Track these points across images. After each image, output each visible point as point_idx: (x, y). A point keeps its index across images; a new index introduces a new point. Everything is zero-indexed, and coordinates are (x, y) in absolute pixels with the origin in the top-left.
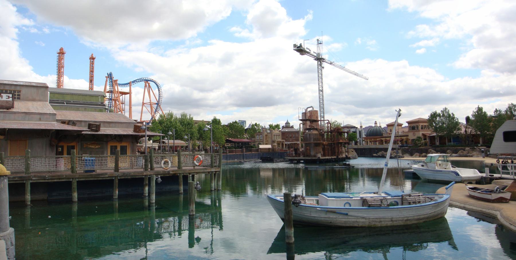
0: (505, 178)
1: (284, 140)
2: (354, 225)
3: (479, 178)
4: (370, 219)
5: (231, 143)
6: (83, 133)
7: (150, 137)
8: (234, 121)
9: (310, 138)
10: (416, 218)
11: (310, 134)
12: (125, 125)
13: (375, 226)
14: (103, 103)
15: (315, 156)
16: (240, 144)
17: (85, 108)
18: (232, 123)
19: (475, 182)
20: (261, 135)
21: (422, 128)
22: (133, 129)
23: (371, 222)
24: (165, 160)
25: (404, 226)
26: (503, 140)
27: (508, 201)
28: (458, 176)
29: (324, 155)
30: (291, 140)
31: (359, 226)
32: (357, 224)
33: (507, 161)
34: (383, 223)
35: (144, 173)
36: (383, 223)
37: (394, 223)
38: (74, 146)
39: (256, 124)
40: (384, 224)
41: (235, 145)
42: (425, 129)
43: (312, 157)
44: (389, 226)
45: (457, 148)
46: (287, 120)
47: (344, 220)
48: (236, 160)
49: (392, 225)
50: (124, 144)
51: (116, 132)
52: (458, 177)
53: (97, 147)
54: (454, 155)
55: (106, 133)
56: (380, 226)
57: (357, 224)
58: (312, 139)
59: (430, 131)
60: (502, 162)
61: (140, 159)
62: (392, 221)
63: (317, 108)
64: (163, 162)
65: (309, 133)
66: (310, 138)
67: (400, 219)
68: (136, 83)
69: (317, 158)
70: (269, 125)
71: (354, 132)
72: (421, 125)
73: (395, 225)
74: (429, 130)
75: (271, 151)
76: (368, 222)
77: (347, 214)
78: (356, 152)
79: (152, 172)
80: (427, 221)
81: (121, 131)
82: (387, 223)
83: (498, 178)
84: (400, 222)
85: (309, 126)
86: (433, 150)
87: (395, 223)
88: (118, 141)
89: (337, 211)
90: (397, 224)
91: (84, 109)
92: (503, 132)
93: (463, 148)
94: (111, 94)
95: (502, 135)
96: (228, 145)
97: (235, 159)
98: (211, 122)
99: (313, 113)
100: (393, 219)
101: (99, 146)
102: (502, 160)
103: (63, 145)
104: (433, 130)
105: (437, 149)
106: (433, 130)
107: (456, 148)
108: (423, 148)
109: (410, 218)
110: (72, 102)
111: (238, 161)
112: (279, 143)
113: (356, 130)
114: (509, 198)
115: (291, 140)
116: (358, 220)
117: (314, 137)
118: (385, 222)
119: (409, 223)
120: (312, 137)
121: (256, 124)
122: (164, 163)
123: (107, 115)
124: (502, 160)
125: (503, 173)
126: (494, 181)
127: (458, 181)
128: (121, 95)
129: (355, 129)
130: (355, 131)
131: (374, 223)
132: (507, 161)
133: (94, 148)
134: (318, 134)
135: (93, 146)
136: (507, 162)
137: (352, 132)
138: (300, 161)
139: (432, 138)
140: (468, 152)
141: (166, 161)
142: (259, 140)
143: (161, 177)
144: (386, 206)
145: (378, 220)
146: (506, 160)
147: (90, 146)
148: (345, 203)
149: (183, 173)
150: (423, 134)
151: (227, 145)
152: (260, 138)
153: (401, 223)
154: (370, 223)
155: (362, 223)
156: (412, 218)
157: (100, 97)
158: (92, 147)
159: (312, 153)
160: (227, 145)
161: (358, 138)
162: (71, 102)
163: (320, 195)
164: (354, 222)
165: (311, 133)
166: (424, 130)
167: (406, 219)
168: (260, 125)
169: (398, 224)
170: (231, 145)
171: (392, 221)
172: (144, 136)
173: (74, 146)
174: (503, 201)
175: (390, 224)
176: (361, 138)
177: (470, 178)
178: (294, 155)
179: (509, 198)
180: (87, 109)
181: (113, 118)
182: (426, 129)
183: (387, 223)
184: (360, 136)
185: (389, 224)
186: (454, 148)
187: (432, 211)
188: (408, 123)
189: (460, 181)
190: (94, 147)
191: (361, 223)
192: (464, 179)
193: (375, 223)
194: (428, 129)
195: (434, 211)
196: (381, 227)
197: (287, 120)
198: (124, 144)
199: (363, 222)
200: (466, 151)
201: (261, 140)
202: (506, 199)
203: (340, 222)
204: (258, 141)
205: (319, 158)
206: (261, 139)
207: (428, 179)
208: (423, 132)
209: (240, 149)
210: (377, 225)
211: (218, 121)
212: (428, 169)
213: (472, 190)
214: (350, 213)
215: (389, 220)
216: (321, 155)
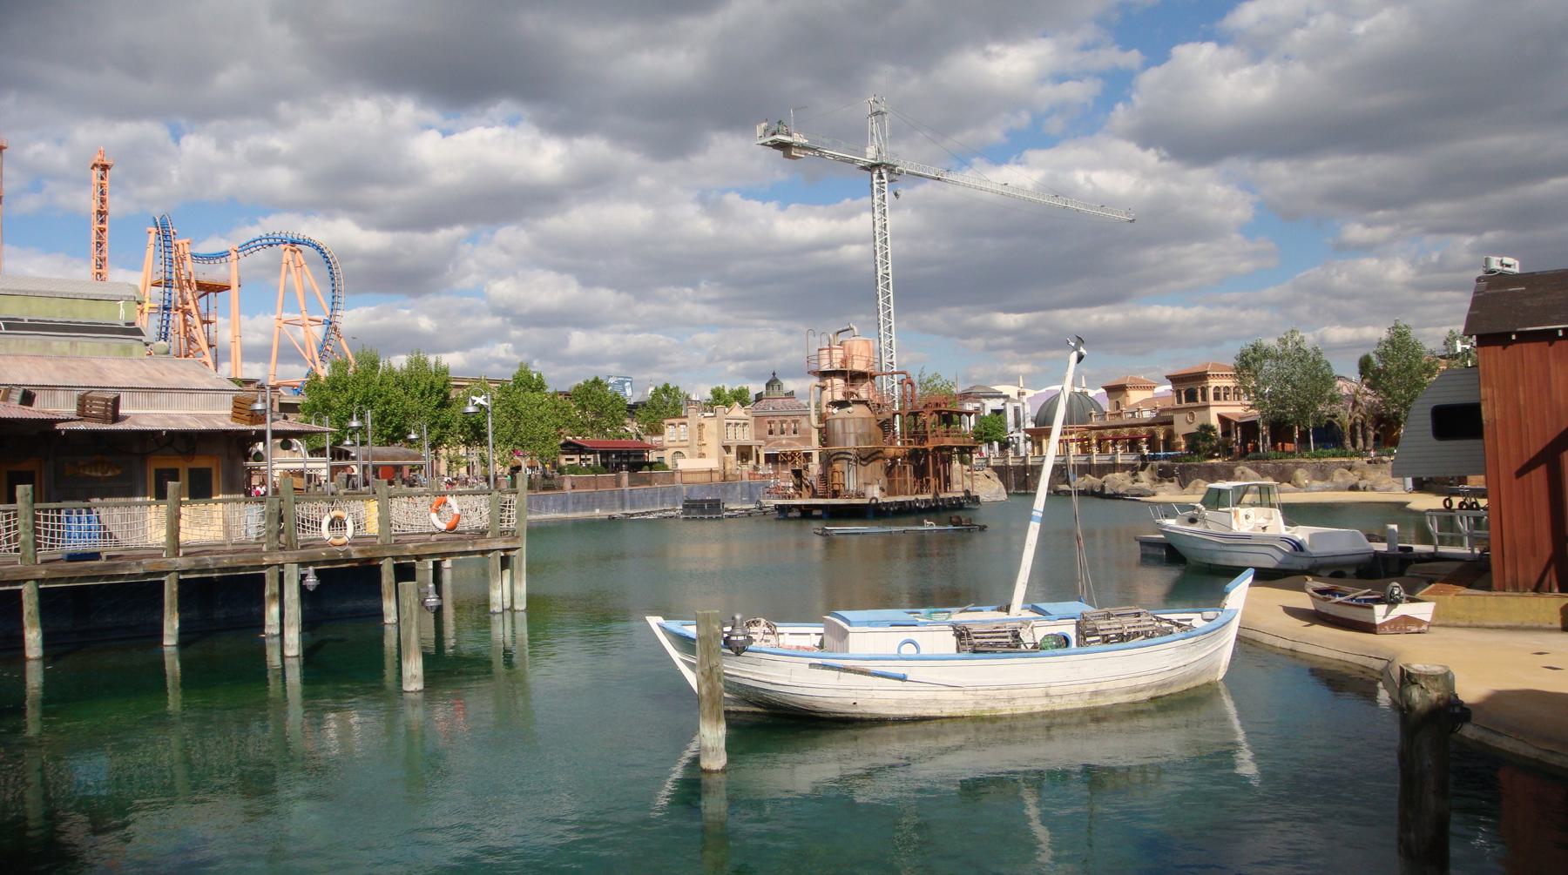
0: (1451, 557)
1: (763, 441)
2: (928, 711)
3: (1367, 556)
4: (978, 693)
5: (580, 454)
6: (59, 426)
7: (285, 439)
8: (591, 379)
9: (844, 432)
10: (1124, 684)
11: (843, 420)
12: (202, 396)
13: (993, 714)
14: (133, 324)
15: (860, 495)
16: (614, 456)
17: (72, 343)
18: (583, 384)
19: (1353, 571)
20: (682, 426)
21: (1217, 397)
22: (230, 412)
23: (981, 702)
24: (333, 514)
25: (1087, 711)
26: (1431, 433)
27: (1424, 627)
28: (1298, 553)
29: (891, 491)
30: (784, 442)
31: (944, 715)
32: (938, 709)
33: (1473, 503)
34: (1019, 702)
35: (265, 559)
36: (1019, 702)
37: (1054, 703)
38: (210, 469)
39: (667, 386)
40: (1022, 707)
41: (595, 459)
42: (1225, 399)
43: (850, 497)
44: (1038, 713)
45: (1325, 460)
46: (774, 374)
47: (896, 695)
48: (597, 511)
49: (1049, 709)
50: (201, 463)
51: (171, 422)
52: (1302, 554)
53: (110, 474)
54: (1317, 484)
55: (138, 428)
56: (1008, 712)
57: (938, 709)
58: (852, 437)
59: (1242, 405)
60: (1461, 505)
61: (252, 510)
62: (1047, 695)
63: (76, 394)
64: (326, 521)
65: (841, 415)
66: (844, 432)
67: (1074, 689)
68: (252, 250)
69: (866, 501)
70: (713, 392)
71: (997, 412)
72: (1214, 385)
73: (1057, 708)
74: (1238, 403)
75: (716, 477)
76: (971, 702)
77: (903, 679)
78: (1001, 478)
79: (291, 555)
80: (1160, 697)
81: (189, 418)
82: (1032, 702)
83: (1425, 556)
84: (1074, 698)
85: (844, 394)
86: (1251, 468)
87: (1059, 705)
88: (181, 453)
89: (873, 669)
90: (1063, 708)
91: (68, 343)
92: (1432, 406)
93: (1346, 460)
94: (167, 290)
95: (1429, 417)
96: (572, 460)
97: (593, 509)
98: (511, 383)
99: (858, 350)
100: (1052, 691)
101: (118, 472)
102: (1461, 499)
103: (176, 466)
104: (1250, 403)
105: (1263, 465)
106: (1250, 403)
107: (1323, 460)
108: (1217, 464)
109: (1103, 687)
110: (26, 322)
111: (605, 514)
112: (745, 450)
113: (1003, 404)
114: (1427, 618)
115: (784, 442)
116: (940, 696)
117: (860, 431)
118: (1026, 700)
119: (1101, 702)
120: (852, 430)
121: (667, 386)
122: (332, 523)
123: (143, 364)
124: (1461, 499)
125: (1442, 542)
126: (1412, 566)
127: (1300, 568)
128: (202, 292)
129: (1002, 401)
130: (1002, 408)
131: (989, 704)
132: (1476, 503)
133: (99, 478)
134: (870, 418)
135: (96, 471)
136: (1475, 506)
137: (992, 410)
138: (811, 511)
139: (1250, 429)
140: (1360, 473)
141: (339, 518)
142: (677, 444)
143: (317, 572)
144: (1030, 646)
145: (1005, 694)
146: (1473, 500)
147: (87, 473)
148: (903, 639)
149: (396, 558)
150: (1222, 418)
151: (567, 460)
152: (679, 437)
153: (1079, 704)
154: (977, 703)
155: (953, 706)
156: (1111, 685)
157: (121, 302)
158: (94, 474)
159: (852, 484)
160: (567, 460)
161: (1012, 433)
162: (22, 320)
163: (828, 617)
164: (927, 701)
165: (850, 416)
166: (1223, 403)
167: (1092, 688)
168: (681, 391)
169: (1069, 707)
170: (581, 459)
171: (1047, 695)
172: (261, 436)
173: (210, 469)
174: (1408, 627)
175: (1042, 705)
176: (1019, 431)
177: (1338, 559)
178: (792, 490)
179: (1427, 618)
180: (79, 345)
181: (163, 374)
182: (1230, 400)
183: (1032, 702)
184: (1017, 424)
185: (1039, 705)
186: (1315, 460)
187: (1178, 661)
188: (1171, 380)
189: (1306, 568)
190: (100, 474)
191: (951, 704)
192: (1320, 561)
193: (994, 705)
194: (1236, 398)
195: (1181, 664)
196: (1013, 717)
197: (774, 374)
198: (201, 463)
199: (955, 701)
200: (1355, 473)
201: (685, 444)
202: (1419, 622)
203: (883, 701)
204: (671, 444)
205: (874, 501)
206: (682, 438)
207: (1210, 564)
208: (1224, 411)
209: (613, 472)
210: (1001, 710)
211: (535, 376)
212: (1208, 530)
213: (1322, 597)
214: (915, 671)
215: (1040, 692)
216: (882, 490)
